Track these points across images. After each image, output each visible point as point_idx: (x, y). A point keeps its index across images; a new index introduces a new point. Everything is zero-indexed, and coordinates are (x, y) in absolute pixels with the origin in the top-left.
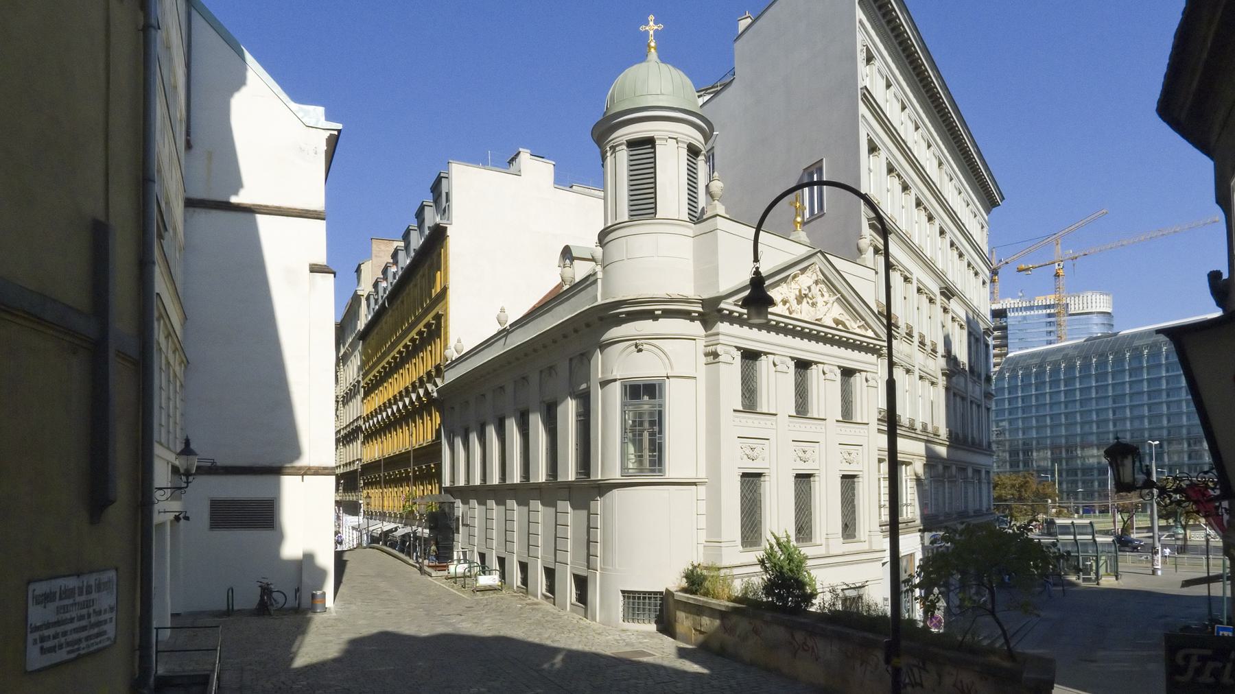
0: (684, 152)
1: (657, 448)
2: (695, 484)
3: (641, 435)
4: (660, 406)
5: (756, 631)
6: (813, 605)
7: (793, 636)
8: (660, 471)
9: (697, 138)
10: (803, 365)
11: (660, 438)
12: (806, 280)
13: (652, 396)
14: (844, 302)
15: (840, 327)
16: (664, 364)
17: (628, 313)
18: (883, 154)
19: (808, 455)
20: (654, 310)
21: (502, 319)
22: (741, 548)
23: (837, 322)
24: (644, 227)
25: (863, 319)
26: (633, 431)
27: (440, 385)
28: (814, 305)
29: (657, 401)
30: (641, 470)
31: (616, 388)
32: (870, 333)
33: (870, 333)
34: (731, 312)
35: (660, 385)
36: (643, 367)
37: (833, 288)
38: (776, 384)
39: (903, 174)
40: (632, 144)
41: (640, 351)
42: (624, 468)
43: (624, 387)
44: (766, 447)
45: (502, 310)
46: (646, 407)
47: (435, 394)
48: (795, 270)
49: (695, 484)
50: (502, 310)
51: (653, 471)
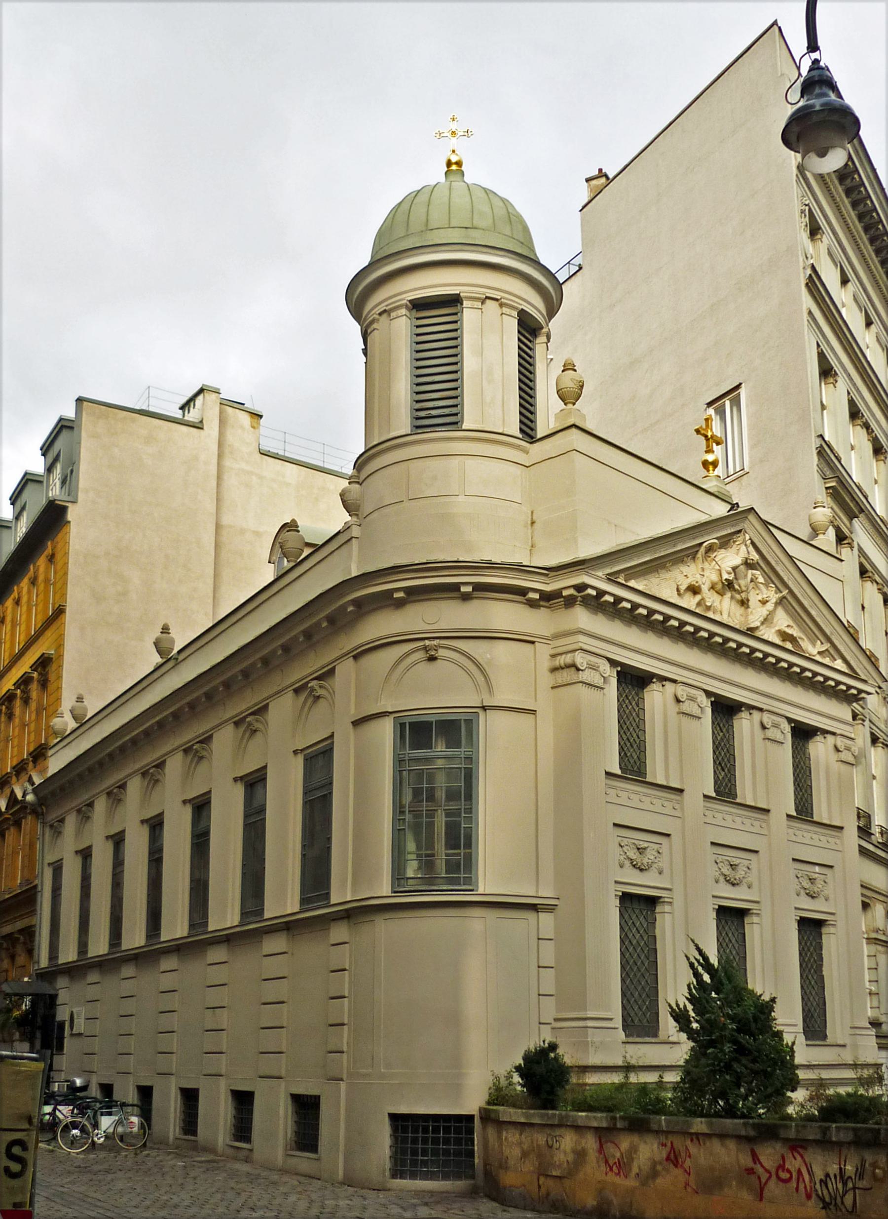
0: (513, 324)
1: (461, 839)
2: (534, 908)
3: (431, 814)
4: (469, 759)
5: (674, 1159)
6: (790, 1102)
7: (755, 1158)
8: (468, 881)
9: (535, 305)
10: (725, 710)
11: (469, 820)
12: (730, 559)
13: (453, 742)
14: (789, 602)
15: (789, 646)
16: (476, 685)
17: (409, 591)
18: (842, 384)
19: (740, 873)
20: (456, 587)
21: (165, 645)
22: (622, 1035)
23: (785, 636)
24: (437, 443)
25: (829, 640)
26: (417, 814)
27: (37, 780)
28: (744, 603)
29: (462, 751)
30: (429, 880)
31: (386, 730)
32: (839, 664)
33: (839, 664)
34: (601, 593)
35: (469, 722)
36: (436, 691)
37: (774, 577)
38: (680, 741)
39: (873, 425)
40: (419, 305)
41: (432, 659)
42: (398, 876)
43: (401, 727)
44: (665, 849)
45: (165, 630)
46: (440, 763)
47: (30, 798)
48: (710, 539)
49: (534, 908)
50: (165, 630)
51: (456, 881)
